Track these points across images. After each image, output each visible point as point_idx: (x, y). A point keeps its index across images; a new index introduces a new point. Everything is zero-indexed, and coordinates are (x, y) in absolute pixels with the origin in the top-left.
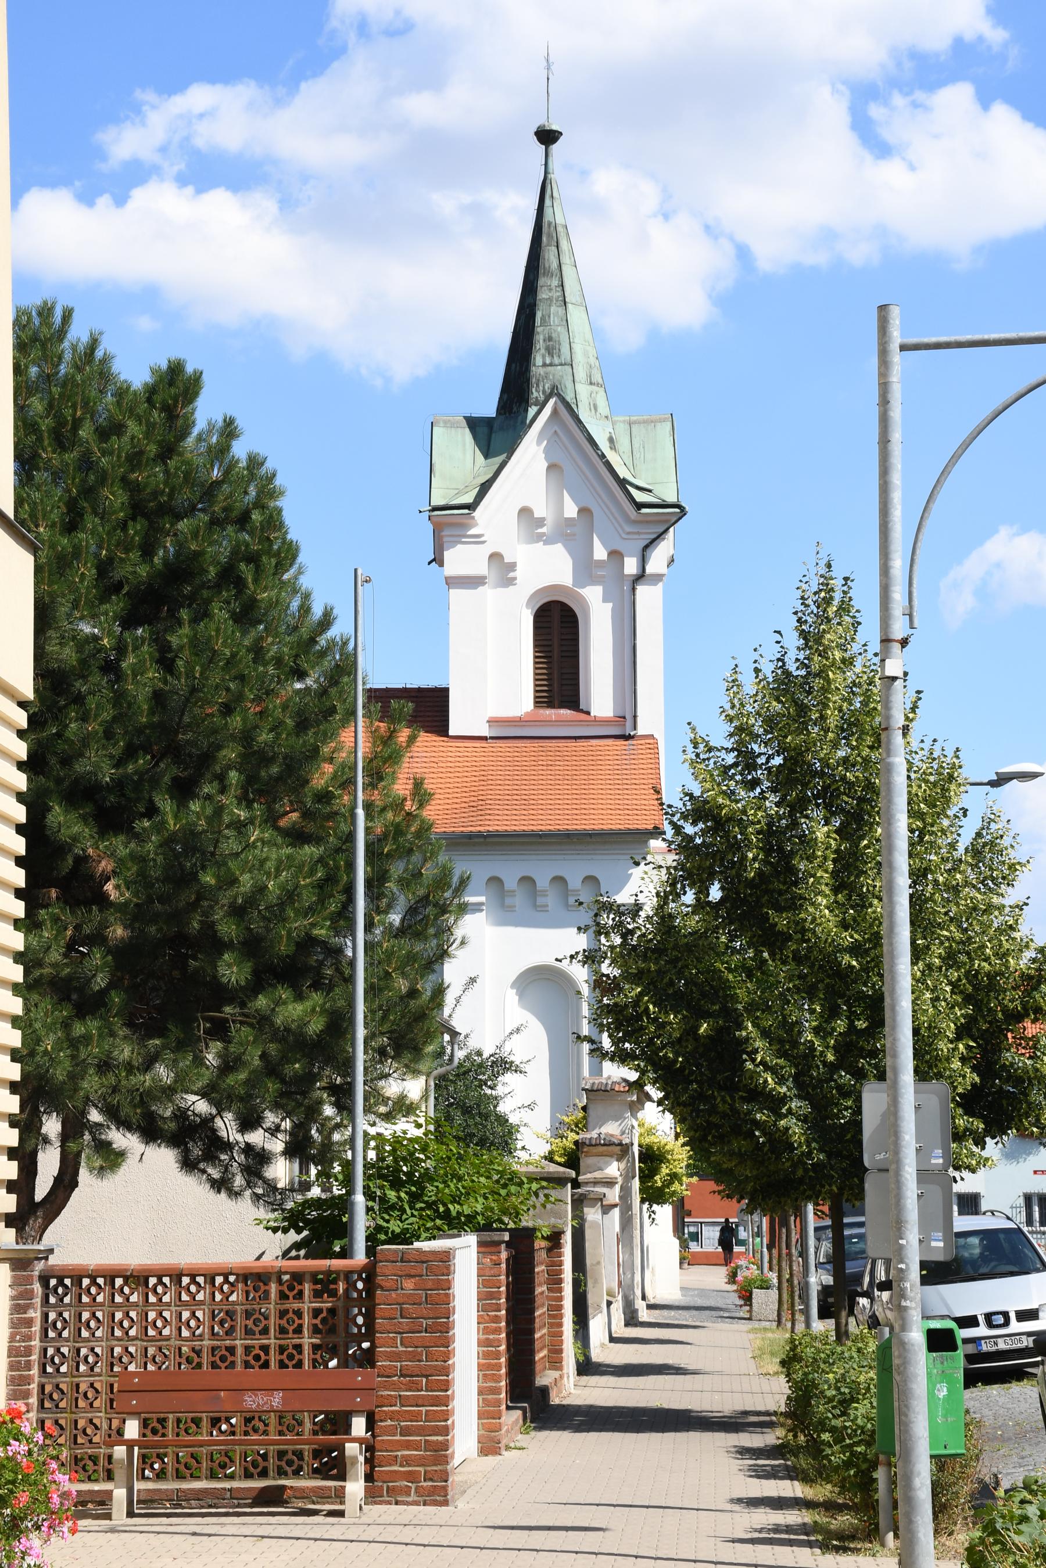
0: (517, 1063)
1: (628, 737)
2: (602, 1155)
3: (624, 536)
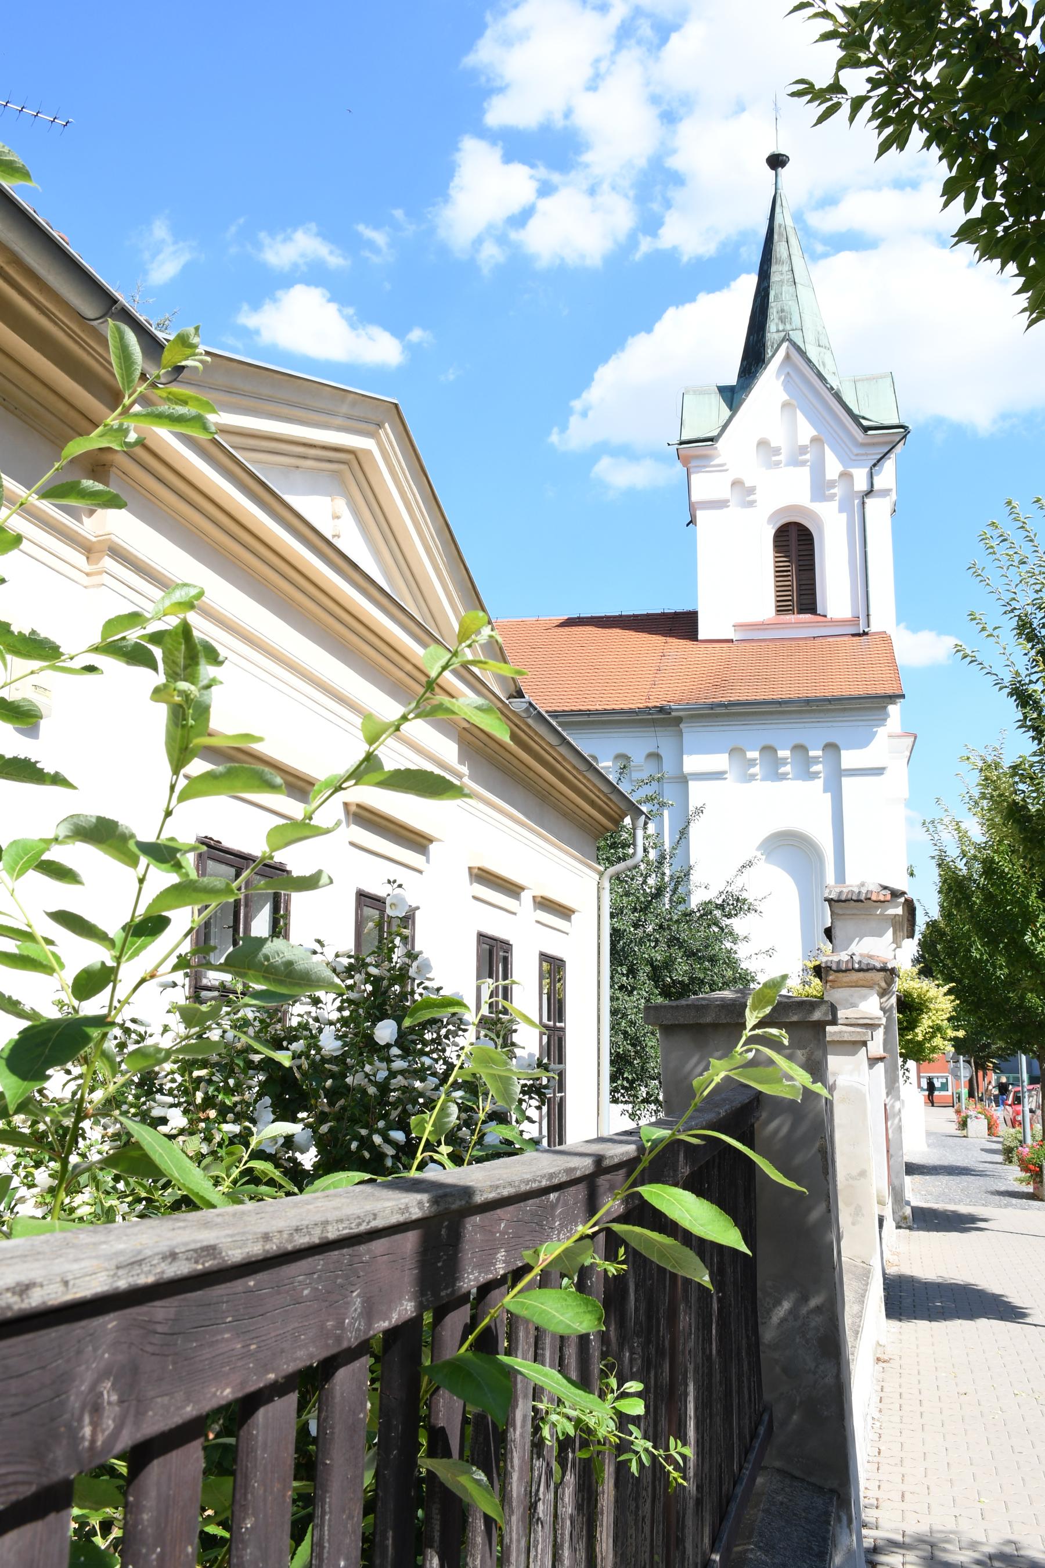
1: (865, 634)
2: (856, 985)
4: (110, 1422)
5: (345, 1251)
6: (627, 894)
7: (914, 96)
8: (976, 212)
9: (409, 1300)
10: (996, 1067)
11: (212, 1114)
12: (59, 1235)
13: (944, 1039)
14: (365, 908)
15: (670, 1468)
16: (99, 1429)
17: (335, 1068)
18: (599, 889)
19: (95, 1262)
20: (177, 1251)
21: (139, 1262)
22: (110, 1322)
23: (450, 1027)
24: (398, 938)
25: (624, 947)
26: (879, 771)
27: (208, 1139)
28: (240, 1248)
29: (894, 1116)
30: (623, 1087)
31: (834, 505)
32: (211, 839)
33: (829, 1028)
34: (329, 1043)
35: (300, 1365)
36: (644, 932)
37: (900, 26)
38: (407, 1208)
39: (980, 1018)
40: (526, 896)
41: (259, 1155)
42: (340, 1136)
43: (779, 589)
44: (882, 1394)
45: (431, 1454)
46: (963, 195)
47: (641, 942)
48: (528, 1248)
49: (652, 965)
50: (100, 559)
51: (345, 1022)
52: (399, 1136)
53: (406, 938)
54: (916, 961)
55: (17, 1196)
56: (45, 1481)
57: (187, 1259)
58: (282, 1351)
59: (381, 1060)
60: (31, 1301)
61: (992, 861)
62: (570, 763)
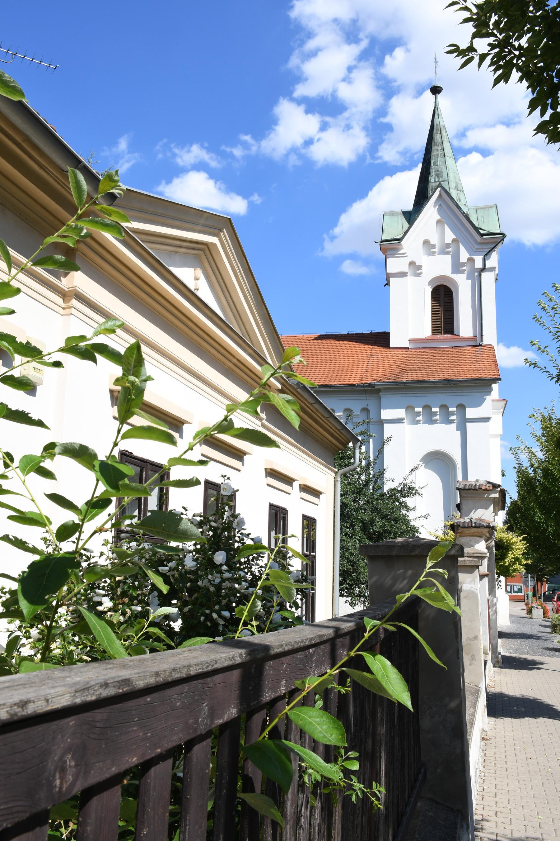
0: (417, 488)
1: (480, 345)
2: (473, 536)
3: (475, 250)
4: (70, 777)
5: (199, 681)
6: (350, 484)
7: (514, 54)
8: (547, 117)
9: (234, 708)
10: (548, 580)
11: (126, 600)
12: (44, 672)
13: (520, 565)
14: (209, 490)
15: (374, 799)
16: (64, 781)
17: (192, 577)
18: (335, 481)
19: (63, 689)
20: (109, 682)
21: (88, 689)
22: (71, 722)
23: (255, 555)
24: (227, 507)
25: (348, 513)
26: (487, 420)
27: (124, 614)
28: (143, 680)
29: (493, 607)
30: (347, 588)
31: (464, 276)
32: (127, 451)
33: (459, 559)
34: (189, 563)
35: (174, 744)
36: (359, 504)
37: (506, 15)
38: (233, 657)
39: (539, 554)
40: (296, 485)
41: (152, 624)
42: (195, 614)
43: (434, 321)
44: (485, 758)
45: (244, 790)
46: (540, 108)
47: (357, 510)
48: (298, 679)
49: (363, 522)
50: (70, 300)
51: (196, 550)
52: (226, 614)
53: (231, 506)
54: (505, 523)
55: (21, 643)
56: (34, 811)
57: (114, 687)
58: (165, 737)
59: (217, 573)
60: (28, 710)
61: (548, 469)
62: (320, 413)
